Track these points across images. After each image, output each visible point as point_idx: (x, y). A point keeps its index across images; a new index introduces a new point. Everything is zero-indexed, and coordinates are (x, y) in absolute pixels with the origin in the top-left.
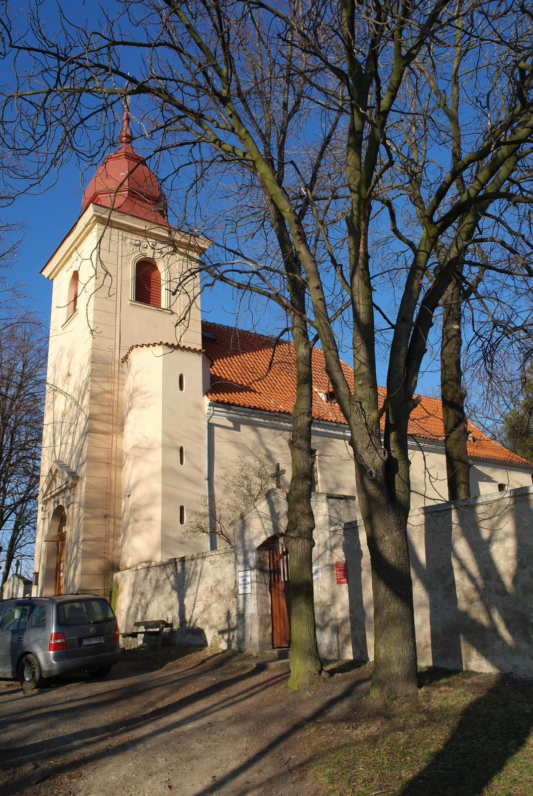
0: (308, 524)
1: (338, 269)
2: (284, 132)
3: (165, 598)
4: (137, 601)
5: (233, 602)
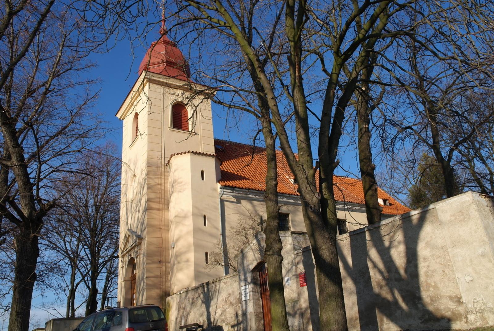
0: (278, 246)
1: (285, 88)
2: (251, 14)
3: (198, 309)
4: (181, 313)
5: (239, 307)
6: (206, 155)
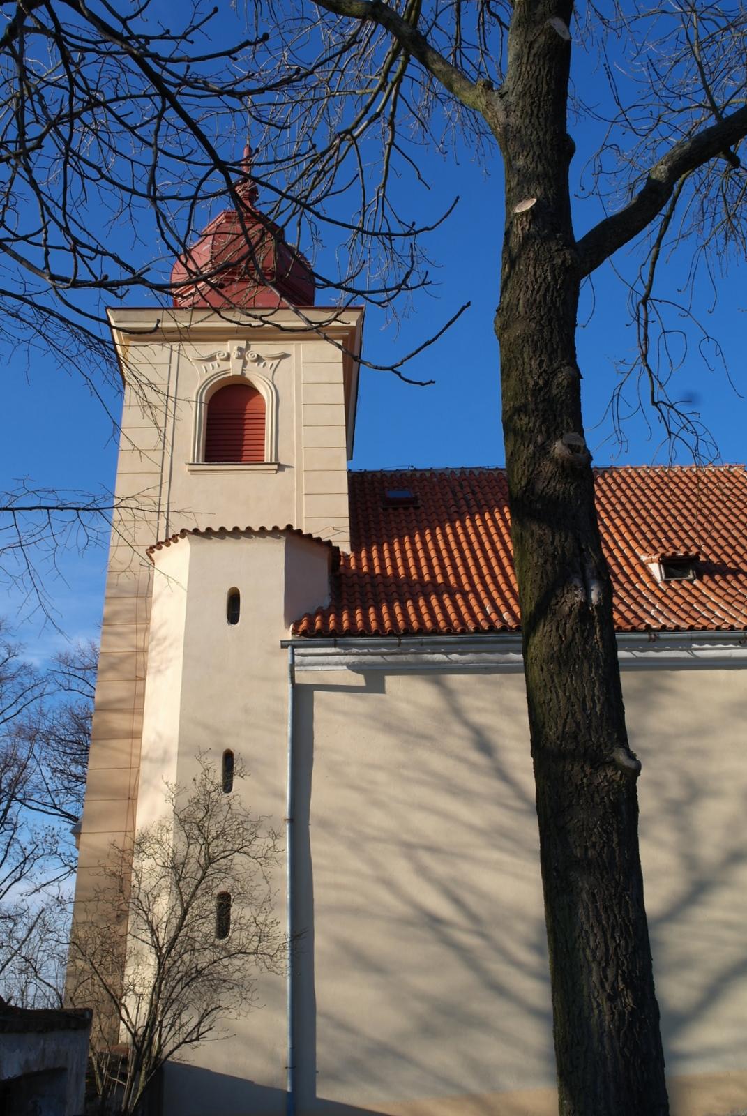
6: (249, 532)
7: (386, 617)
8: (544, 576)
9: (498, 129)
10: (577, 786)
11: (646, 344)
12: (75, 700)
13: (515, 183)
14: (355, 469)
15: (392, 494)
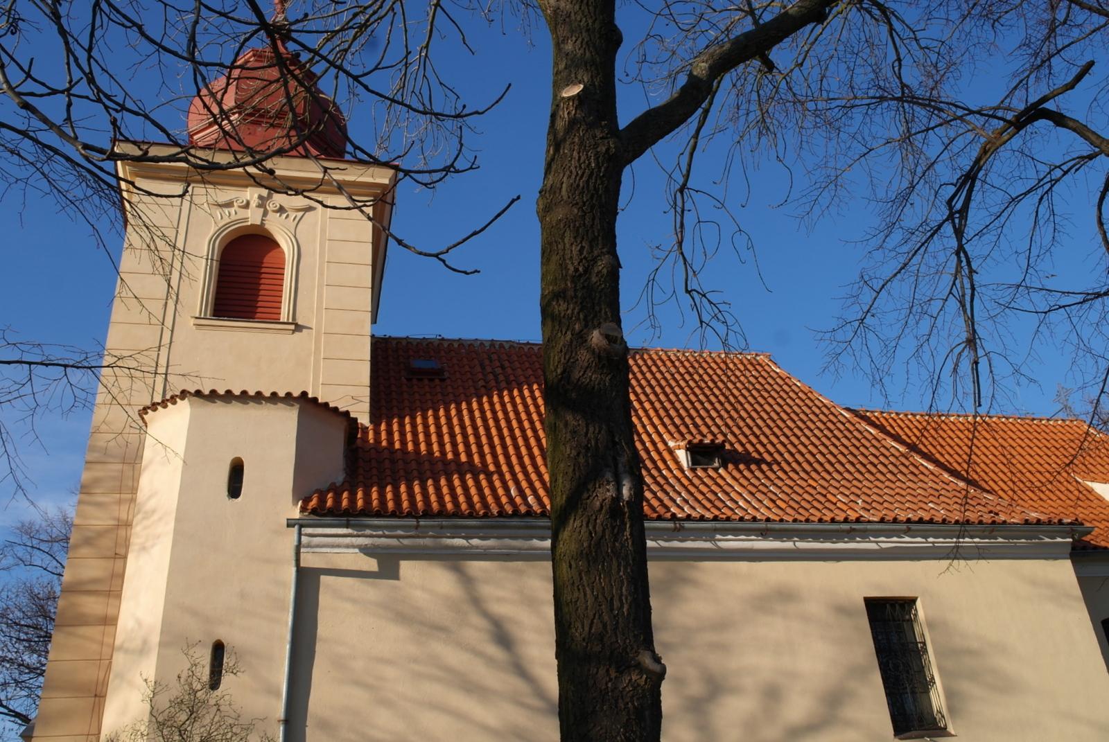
6: (259, 397)
7: (404, 496)
8: (576, 469)
9: (549, 12)
10: (601, 691)
11: (682, 232)
12: (36, 578)
13: (563, 66)
14: (379, 334)
15: (418, 364)
